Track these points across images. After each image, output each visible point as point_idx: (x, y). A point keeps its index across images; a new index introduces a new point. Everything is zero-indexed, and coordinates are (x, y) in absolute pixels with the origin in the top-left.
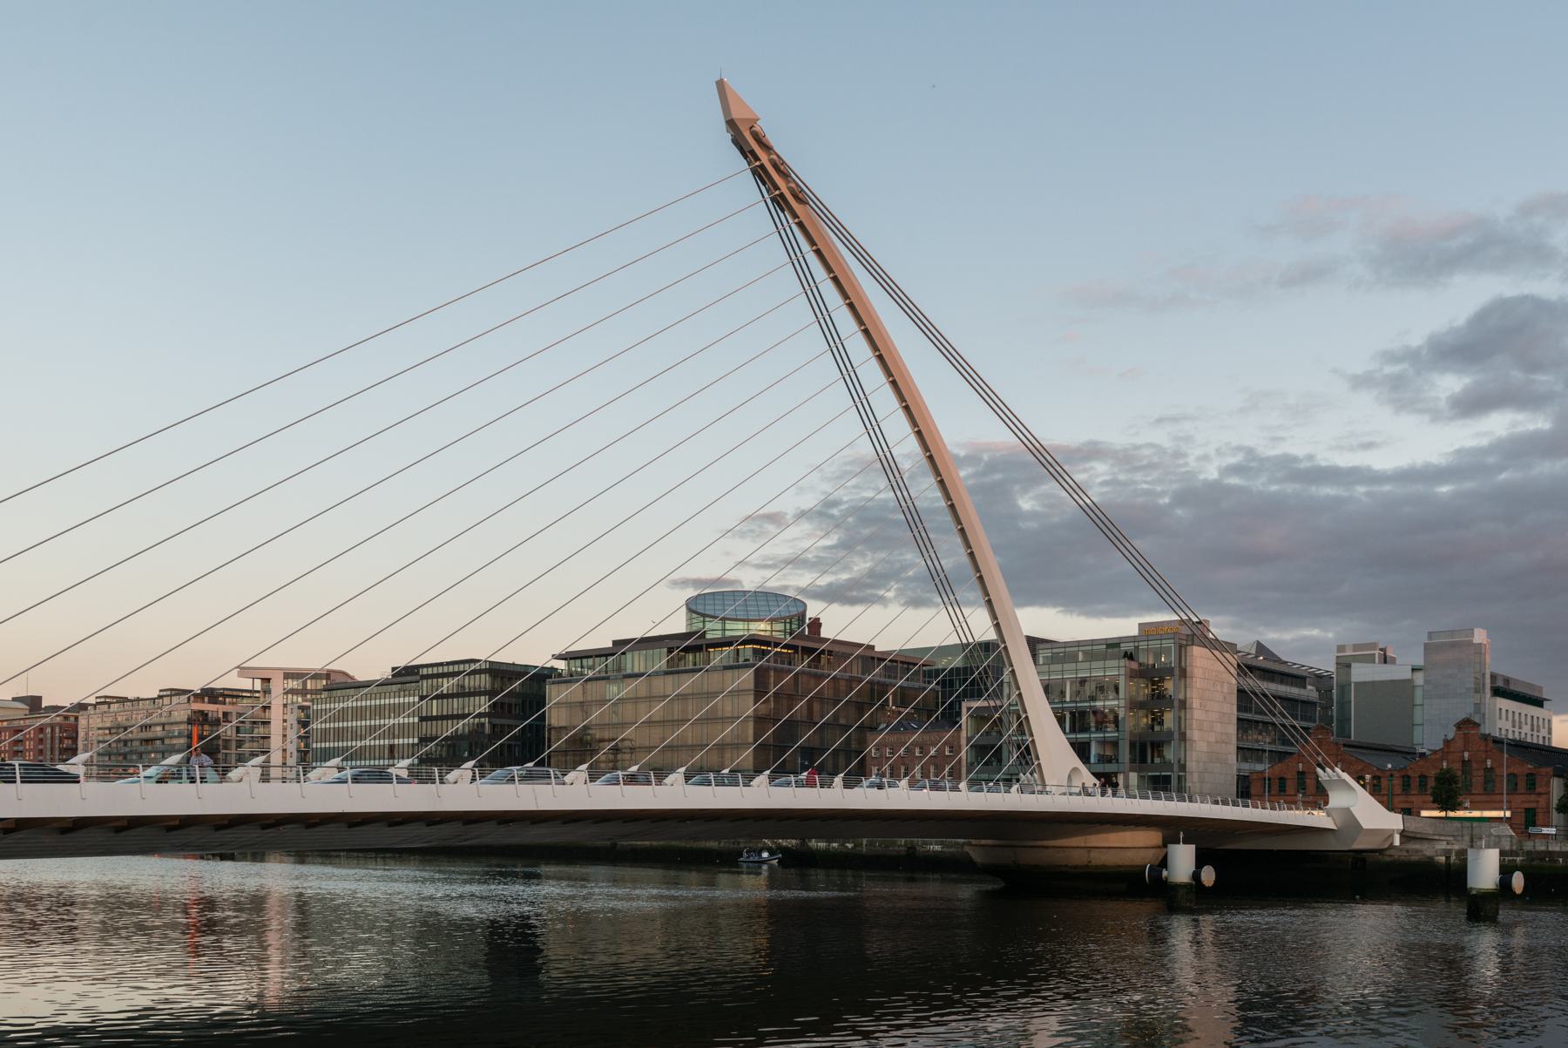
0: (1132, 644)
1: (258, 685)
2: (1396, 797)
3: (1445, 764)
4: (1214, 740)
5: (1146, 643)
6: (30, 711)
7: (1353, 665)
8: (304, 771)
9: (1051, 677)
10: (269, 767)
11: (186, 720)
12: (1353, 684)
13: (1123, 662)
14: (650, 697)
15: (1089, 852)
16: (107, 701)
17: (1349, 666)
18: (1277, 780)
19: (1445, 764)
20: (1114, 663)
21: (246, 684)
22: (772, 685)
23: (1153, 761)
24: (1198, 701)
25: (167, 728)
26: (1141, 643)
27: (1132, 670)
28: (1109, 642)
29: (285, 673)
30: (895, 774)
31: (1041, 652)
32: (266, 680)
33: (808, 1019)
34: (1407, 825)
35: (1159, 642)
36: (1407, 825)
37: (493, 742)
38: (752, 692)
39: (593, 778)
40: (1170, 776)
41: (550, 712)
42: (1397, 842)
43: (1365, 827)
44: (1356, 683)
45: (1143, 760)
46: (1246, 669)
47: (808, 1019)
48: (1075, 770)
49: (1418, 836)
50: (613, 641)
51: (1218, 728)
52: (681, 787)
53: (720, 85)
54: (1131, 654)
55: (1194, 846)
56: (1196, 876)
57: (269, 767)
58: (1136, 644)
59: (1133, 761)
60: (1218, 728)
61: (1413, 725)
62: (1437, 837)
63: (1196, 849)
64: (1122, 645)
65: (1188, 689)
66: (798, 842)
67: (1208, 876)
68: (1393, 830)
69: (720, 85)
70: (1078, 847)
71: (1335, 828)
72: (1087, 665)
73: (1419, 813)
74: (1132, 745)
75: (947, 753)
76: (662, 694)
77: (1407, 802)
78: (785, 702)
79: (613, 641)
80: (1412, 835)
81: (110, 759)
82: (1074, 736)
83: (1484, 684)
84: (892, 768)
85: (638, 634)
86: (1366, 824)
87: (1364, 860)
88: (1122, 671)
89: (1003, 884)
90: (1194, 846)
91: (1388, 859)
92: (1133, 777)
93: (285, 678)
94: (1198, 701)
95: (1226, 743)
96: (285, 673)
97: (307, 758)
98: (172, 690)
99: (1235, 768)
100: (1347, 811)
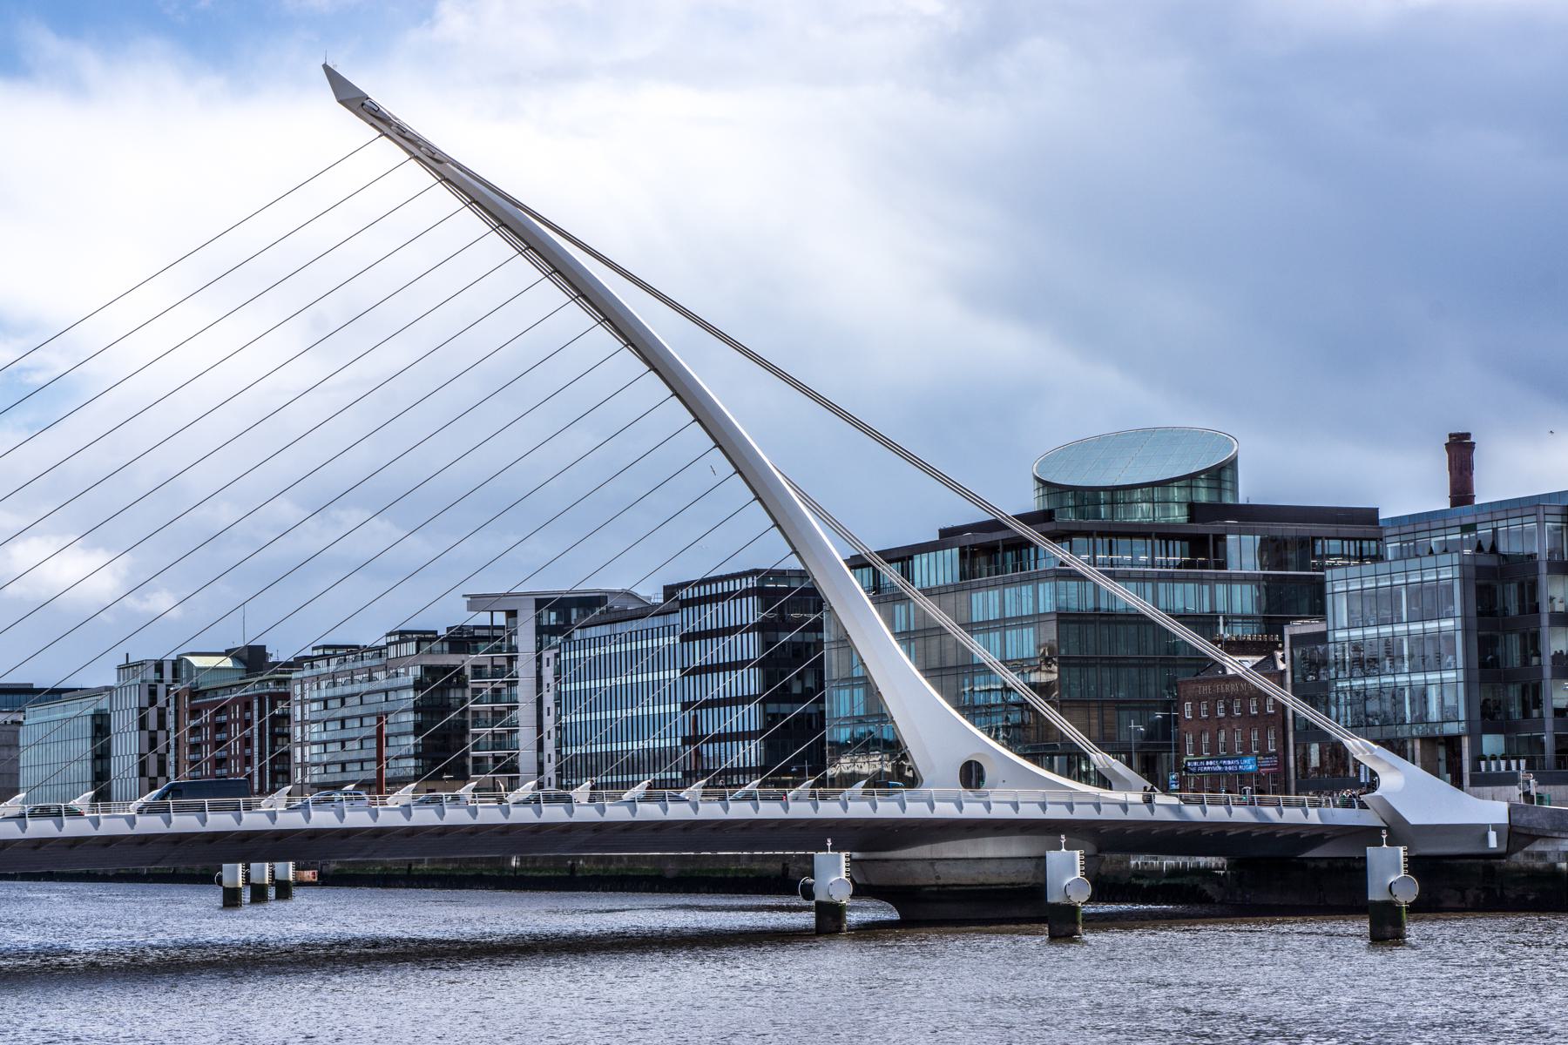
1: (500, 619)
6: (248, 671)
11: (412, 683)
14: (925, 630)
16: (332, 651)
21: (483, 618)
25: (392, 696)
29: (536, 599)
32: (512, 614)
33: (268, 740)
34: (1515, 817)
36: (1515, 817)
38: (1055, 617)
41: (828, 654)
47: (268, 740)
50: (940, 531)
53: (127, 655)
61: (761, 664)
62: (1556, 834)
64: (1479, 526)
69: (127, 655)
72: (1399, 565)
76: (1041, 624)
79: (940, 531)
81: (410, 865)
83: (215, 669)
85: (699, 577)
91: (1512, 865)
93: (537, 609)
96: (536, 599)
97: (569, 771)
98: (402, 633)
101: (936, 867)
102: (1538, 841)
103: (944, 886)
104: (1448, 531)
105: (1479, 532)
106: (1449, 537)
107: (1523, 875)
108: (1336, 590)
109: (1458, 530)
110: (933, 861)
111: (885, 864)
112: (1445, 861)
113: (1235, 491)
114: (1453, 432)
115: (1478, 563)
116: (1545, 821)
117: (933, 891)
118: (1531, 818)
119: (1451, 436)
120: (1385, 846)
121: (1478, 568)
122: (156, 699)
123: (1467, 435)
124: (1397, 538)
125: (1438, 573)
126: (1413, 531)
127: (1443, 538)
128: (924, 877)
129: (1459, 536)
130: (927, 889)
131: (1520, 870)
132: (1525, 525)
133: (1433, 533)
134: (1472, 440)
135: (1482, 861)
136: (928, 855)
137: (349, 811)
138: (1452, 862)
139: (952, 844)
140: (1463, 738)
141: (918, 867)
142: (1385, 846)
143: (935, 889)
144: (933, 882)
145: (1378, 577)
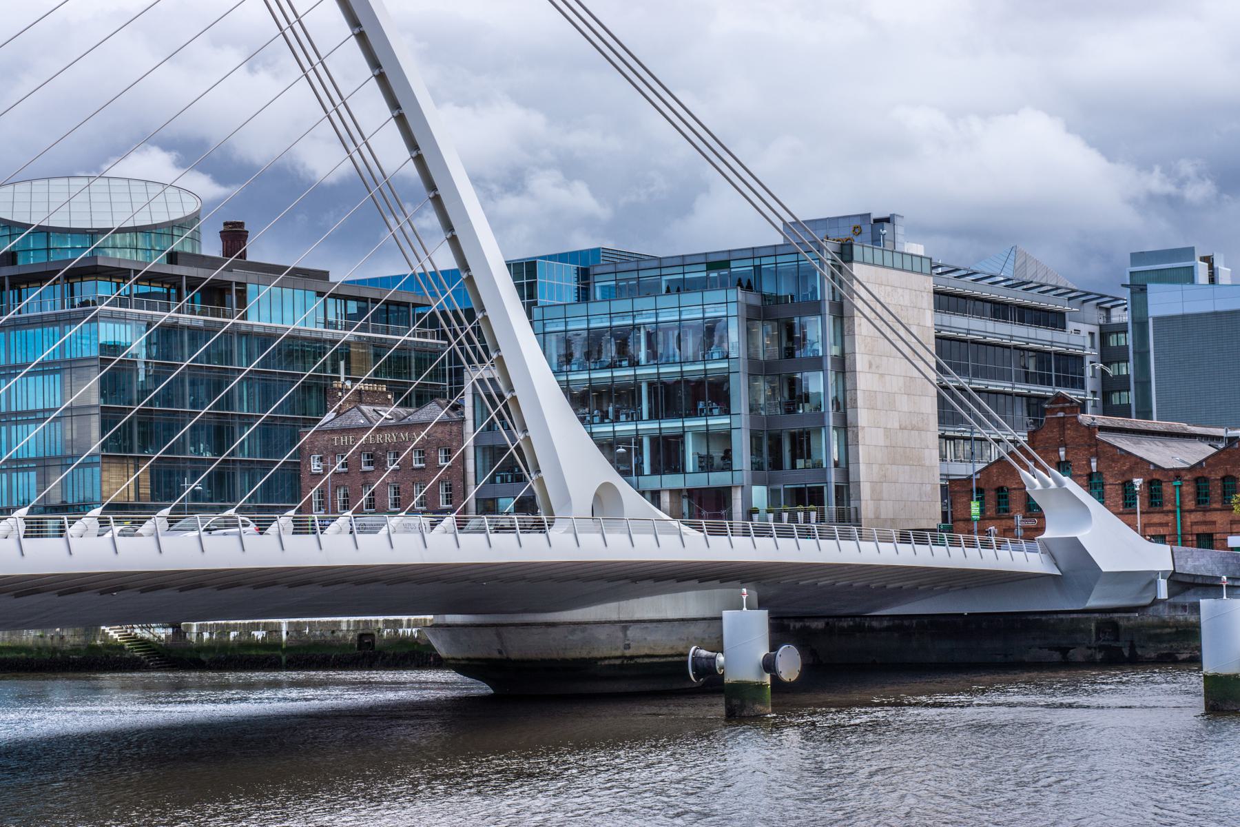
0: (750, 262)
2: (1187, 514)
3: (1062, 453)
4: (897, 425)
5: (772, 260)
7: (1151, 287)
8: (321, 529)
9: (614, 324)
10: (554, 518)
12: (1151, 321)
13: (736, 294)
15: (625, 629)
17: (1143, 290)
18: (993, 493)
19: (1062, 453)
20: (719, 295)
22: (256, 353)
23: (794, 466)
24: (866, 358)
26: (764, 261)
27: (749, 306)
28: (712, 259)
30: (331, 510)
31: (597, 278)
35: (680, 270)
37: (496, 429)
39: (461, 525)
40: (823, 487)
42: (1163, 593)
43: (1103, 570)
44: (1156, 319)
45: (777, 464)
46: (946, 301)
48: (607, 487)
49: (1200, 581)
51: (903, 404)
52: (451, 537)
54: (749, 282)
55: (766, 612)
56: (769, 665)
57: (554, 518)
58: (757, 262)
59: (756, 467)
60: (903, 404)
63: (769, 613)
64: (733, 264)
65: (846, 338)
66: (170, 631)
67: (790, 664)
68: (1157, 573)
70: (605, 622)
71: (1058, 573)
73: (1226, 540)
74: (755, 437)
75: (365, 468)
77: (1205, 523)
78: (145, 394)
80: (1188, 580)
82: (656, 426)
84: (322, 494)
86: (1107, 563)
87: (1115, 626)
88: (733, 310)
89: (491, 691)
90: (766, 612)
92: (759, 495)
94: (866, 358)
95: (919, 430)
99: (937, 473)
100: (1075, 544)
101: (628, 632)
102: (1192, 591)
103: (632, 658)
104: (687, 269)
105: (732, 270)
106: (687, 276)
107: (1168, 630)
108: (547, 330)
109: (704, 267)
110: (625, 625)
111: (550, 630)
112: (1031, 617)
113: (200, 249)
114: (229, 220)
115: (749, 302)
116: (1214, 567)
117: (614, 665)
118: (1197, 563)
119: (226, 224)
120: (745, 609)
121: (749, 306)
122: (245, 298)
123: (241, 224)
124: (612, 277)
125: (657, 315)
126: (635, 268)
127: (681, 276)
128: (607, 647)
129: (704, 274)
130: (606, 662)
131: (1164, 624)
132: (800, 263)
133: (664, 271)
134: (246, 229)
135: (1097, 615)
136: (614, 617)
137: (358, 533)
138: (1044, 618)
139: (647, 600)
140: (733, 490)
141: (602, 634)
142: (745, 609)
143: (618, 662)
144: (618, 653)
145: (567, 320)
